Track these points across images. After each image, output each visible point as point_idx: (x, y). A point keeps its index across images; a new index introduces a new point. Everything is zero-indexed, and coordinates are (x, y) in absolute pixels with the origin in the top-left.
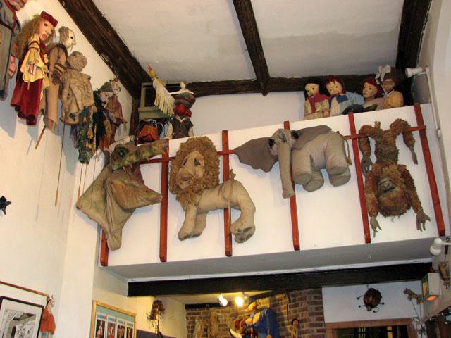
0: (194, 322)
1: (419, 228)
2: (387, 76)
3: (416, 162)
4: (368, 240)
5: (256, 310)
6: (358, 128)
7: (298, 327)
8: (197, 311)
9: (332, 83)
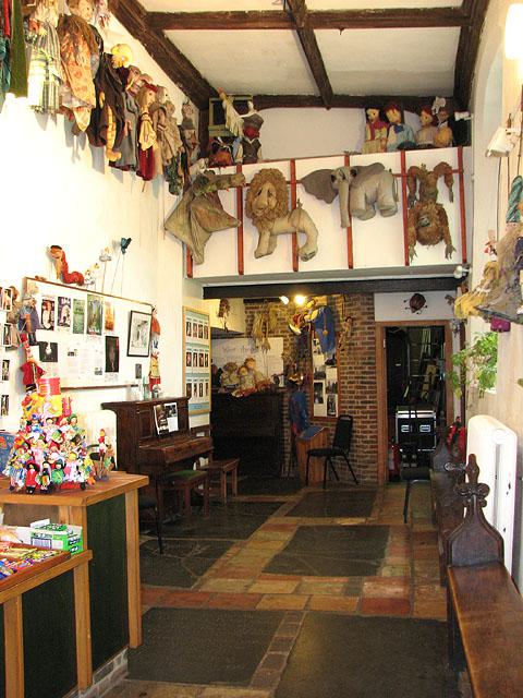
0: (253, 316)
1: (446, 257)
2: (441, 109)
3: (452, 200)
4: (407, 264)
5: (314, 307)
6: (408, 168)
7: (352, 324)
8: (255, 305)
9: (391, 111)
